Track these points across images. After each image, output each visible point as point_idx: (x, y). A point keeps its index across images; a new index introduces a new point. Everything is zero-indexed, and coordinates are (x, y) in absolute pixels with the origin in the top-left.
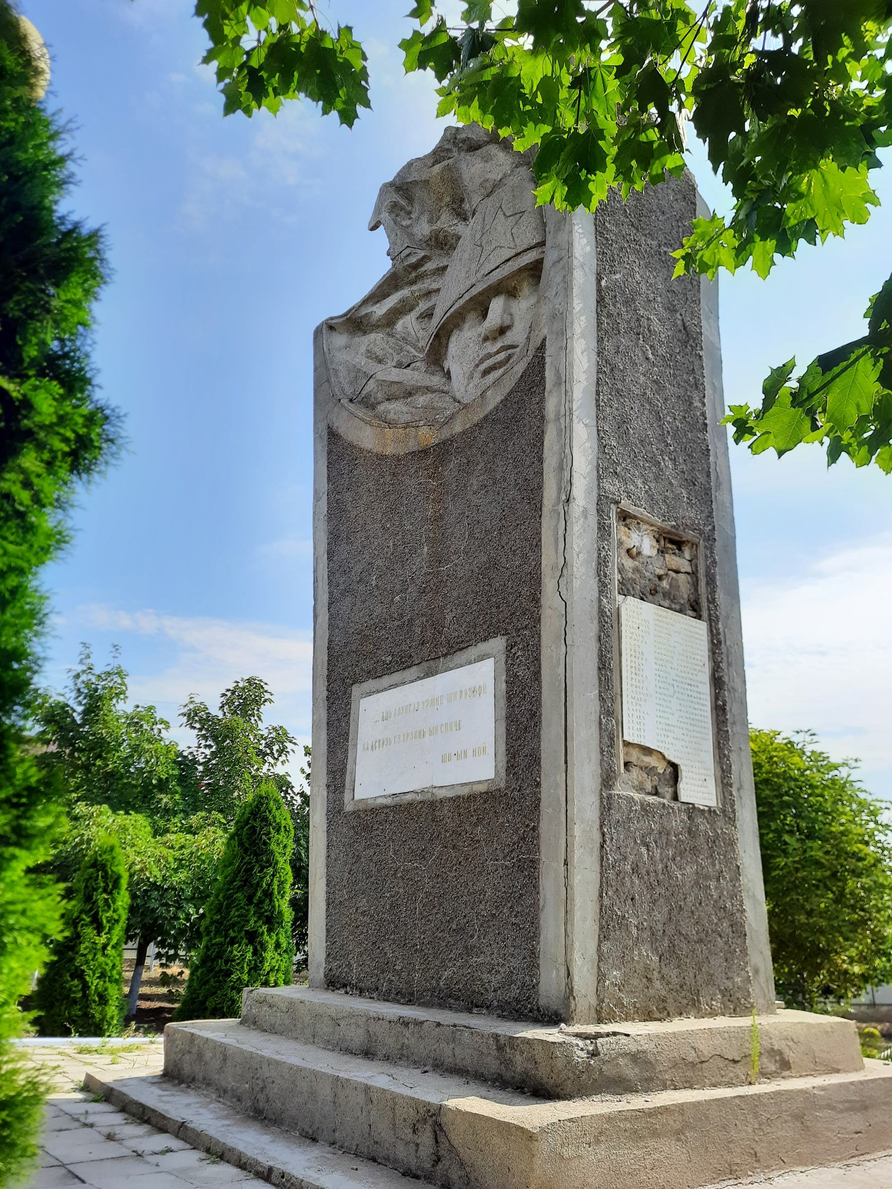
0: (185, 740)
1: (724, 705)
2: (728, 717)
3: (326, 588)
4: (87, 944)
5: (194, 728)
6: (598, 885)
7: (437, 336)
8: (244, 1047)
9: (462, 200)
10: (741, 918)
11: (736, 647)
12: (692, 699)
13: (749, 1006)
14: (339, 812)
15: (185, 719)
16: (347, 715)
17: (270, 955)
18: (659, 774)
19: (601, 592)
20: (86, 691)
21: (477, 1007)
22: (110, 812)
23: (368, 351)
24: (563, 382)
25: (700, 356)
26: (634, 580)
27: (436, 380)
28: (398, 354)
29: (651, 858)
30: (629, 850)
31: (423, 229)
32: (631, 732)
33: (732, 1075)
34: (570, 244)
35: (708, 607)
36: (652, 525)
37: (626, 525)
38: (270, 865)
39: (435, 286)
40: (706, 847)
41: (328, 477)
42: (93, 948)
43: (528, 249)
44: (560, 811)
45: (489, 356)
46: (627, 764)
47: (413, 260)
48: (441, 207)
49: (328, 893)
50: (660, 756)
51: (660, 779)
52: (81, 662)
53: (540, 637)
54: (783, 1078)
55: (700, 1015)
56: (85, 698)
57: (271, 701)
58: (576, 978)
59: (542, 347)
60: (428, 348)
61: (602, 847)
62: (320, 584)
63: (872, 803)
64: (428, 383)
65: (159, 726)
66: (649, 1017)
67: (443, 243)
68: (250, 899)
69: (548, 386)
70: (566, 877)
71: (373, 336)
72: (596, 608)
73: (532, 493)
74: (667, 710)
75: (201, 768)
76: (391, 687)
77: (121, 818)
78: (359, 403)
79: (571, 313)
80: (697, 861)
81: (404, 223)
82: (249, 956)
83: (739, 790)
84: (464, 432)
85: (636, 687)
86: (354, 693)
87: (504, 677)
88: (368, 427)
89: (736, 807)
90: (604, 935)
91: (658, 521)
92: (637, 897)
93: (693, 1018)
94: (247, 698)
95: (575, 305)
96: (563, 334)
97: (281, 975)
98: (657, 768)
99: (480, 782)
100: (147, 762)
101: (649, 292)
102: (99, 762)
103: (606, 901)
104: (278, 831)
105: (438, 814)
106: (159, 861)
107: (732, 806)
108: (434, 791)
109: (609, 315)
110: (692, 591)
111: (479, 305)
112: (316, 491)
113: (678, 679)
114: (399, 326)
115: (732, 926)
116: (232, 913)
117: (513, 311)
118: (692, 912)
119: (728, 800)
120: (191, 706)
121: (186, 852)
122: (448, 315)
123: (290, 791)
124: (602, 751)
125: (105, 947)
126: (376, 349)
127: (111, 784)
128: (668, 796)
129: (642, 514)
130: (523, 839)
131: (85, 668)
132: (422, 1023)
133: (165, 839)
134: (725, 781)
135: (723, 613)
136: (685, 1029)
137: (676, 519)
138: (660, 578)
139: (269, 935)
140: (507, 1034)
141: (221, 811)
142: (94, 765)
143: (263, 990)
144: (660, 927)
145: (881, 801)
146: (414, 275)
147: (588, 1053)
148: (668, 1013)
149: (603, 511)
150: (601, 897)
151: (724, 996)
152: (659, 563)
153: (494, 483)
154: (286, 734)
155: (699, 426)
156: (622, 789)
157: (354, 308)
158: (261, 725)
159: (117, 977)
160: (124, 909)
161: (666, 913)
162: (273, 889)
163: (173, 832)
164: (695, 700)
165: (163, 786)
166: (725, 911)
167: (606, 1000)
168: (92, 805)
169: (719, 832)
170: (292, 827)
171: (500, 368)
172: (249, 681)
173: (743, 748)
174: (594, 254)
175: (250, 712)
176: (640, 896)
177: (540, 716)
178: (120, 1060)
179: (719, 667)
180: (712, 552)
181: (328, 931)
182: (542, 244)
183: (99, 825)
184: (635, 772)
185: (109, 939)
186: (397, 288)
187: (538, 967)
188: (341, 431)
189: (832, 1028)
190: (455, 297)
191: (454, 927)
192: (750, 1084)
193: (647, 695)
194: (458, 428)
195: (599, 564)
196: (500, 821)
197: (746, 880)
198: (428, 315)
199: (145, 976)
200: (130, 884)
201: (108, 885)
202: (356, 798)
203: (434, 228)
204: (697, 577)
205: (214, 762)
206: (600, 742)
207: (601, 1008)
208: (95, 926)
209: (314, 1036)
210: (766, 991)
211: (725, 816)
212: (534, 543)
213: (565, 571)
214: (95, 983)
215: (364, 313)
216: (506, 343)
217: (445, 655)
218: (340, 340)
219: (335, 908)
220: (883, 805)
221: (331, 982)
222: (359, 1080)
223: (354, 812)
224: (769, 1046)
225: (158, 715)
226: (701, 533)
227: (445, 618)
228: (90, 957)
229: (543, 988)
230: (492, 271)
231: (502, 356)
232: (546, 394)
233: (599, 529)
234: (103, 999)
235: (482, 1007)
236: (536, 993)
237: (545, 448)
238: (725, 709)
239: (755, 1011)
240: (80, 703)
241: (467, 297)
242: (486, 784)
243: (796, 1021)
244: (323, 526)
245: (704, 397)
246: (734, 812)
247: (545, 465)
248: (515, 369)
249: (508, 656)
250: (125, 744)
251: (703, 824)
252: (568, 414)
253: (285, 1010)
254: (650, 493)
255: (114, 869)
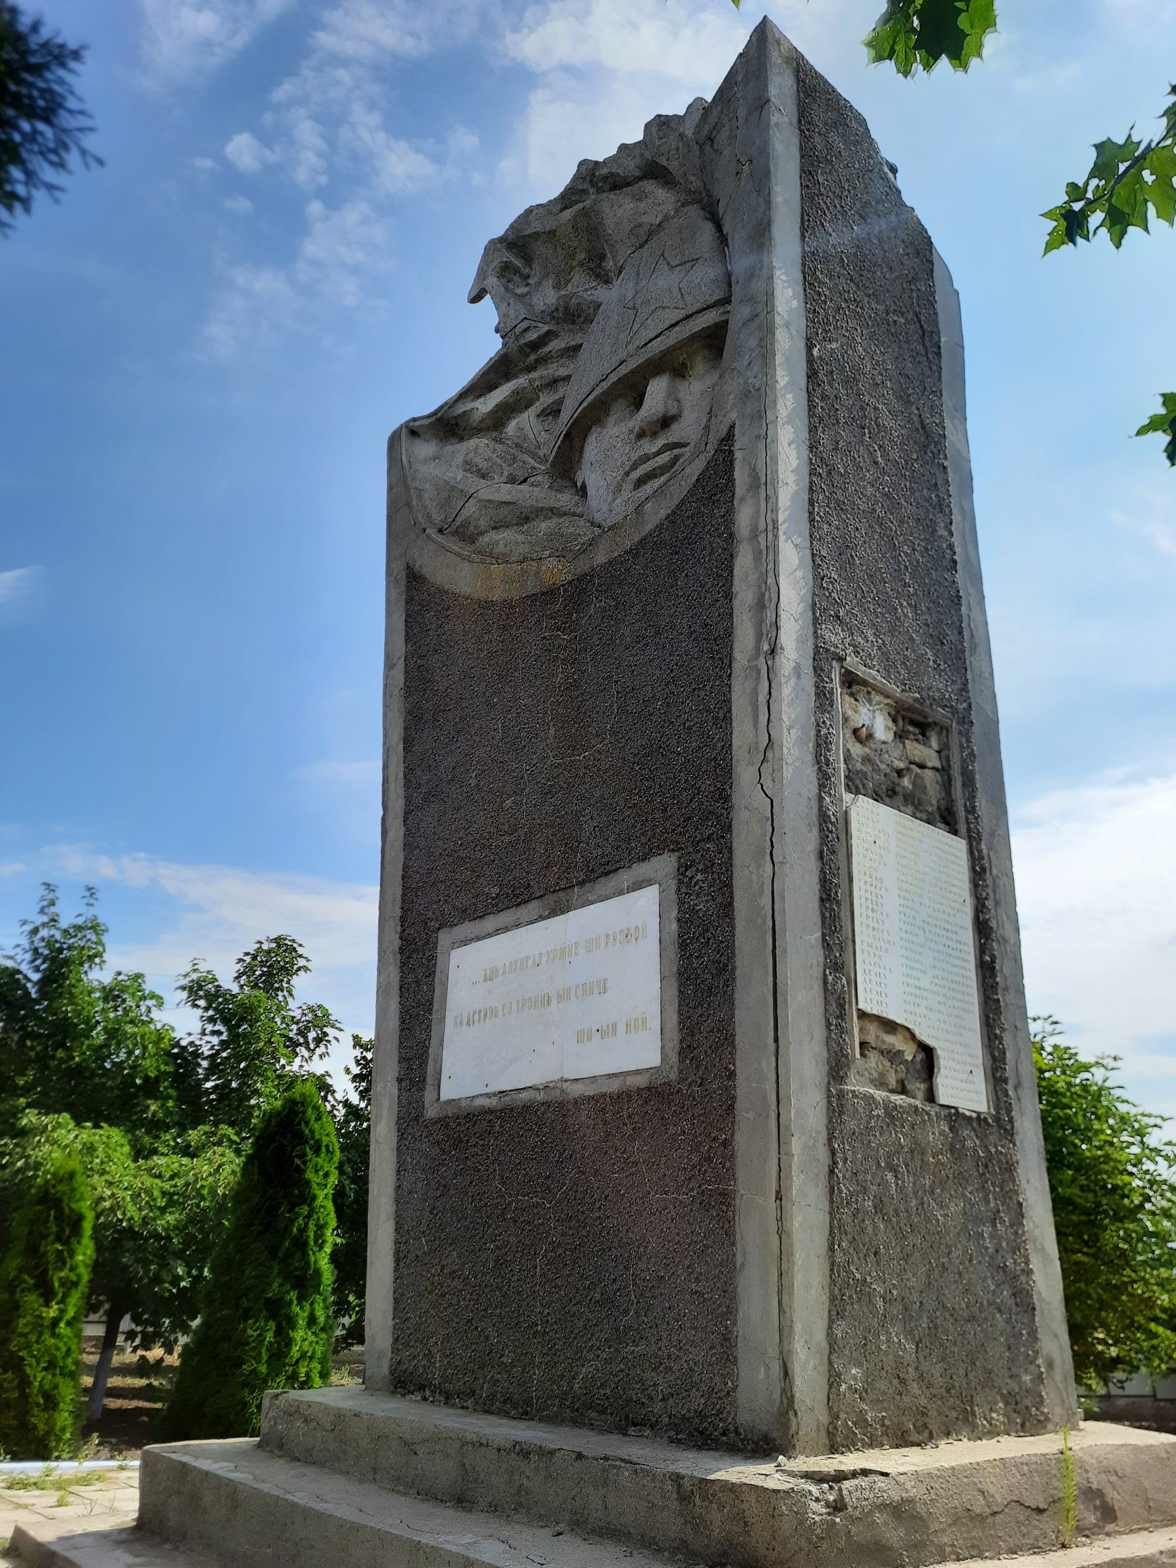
0: (185, 1023)
1: (993, 961)
2: (998, 979)
3: (401, 791)
4: (29, 1318)
5: (197, 1006)
6: (827, 1232)
7: (568, 435)
8: (265, 1487)
9: (603, 257)
10: (1027, 1283)
11: (1005, 878)
12: (950, 951)
13: (1042, 1418)
14: (416, 1119)
15: (185, 994)
16: (431, 974)
17: (302, 1338)
18: (906, 1061)
19: (821, 786)
20: (46, 952)
21: (635, 1425)
22: (72, 1125)
23: (466, 462)
24: (762, 484)
25: (945, 468)
26: (865, 774)
27: (566, 499)
28: (509, 466)
29: (901, 1189)
30: (869, 1177)
31: (547, 297)
32: (869, 996)
33: (1036, 1532)
34: (770, 295)
35: (967, 818)
36: (887, 697)
37: (852, 695)
38: (304, 1202)
39: (563, 372)
40: (976, 1173)
41: (407, 635)
42: (38, 1325)
43: (704, 309)
44: (768, 1116)
45: (646, 458)
46: (863, 1045)
47: (533, 336)
48: (572, 268)
49: (397, 1242)
50: (908, 1035)
51: (907, 1069)
52: (42, 911)
53: (731, 852)
54: (1108, 1534)
55: (977, 1435)
56: (44, 963)
57: (306, 969)
58: (798, 1381)
59: (729, 437)
60: (554, 454)
61: (832, 1172)
62: (392, 786)
63: (1139, 1118)
64: (552, 503)
65: (150, 1003)
66: (902, 1440)
67: (575, 316)
68: (273, 1252)
69: (739, 491)
70: (780, 1220)
71: (474, 442)
72: (815, 810)
73: (717, 644)
74: (916, 965)
75: (205, 1064)
76: (498, 931)
77: (88, 1133)
78: (453, 534)
79: (773, 388)
80: (964, 1196)
81: (518, 291)
82: (270, 1336)
83: (1016, 1088)
84: (610, 563)
85: (874, 929)
86: (440, 943)
87: (674, 913)
88: (467, 564)
89: (1013, 1113)
90: (837, 1310)
91: (897, 691)
92: (882, 1251)
93: (965, 1440)
94: (274, 965)
95: (779, 378)
96: (760, 418)
97: (316, 1365)
98: (903, 1052)
99: (637, 1072)
100: (130, 1053)
101: (875, 373)
102: (60, 1054)
103: (839, 1257)
104: (317, 1151)
105: (570, 1121)
106: (139, 1195)
107: (1009, 1111)
108: (565, 1085)
109: (824, 397)
110: (943, 795)
111: (631, 390)
112: (388, 657)
113: (931, 921)
114: (511, 428)
115: (1014, 1295)
116: (247, 1273)
117: (681, 395)
118: (960, 1273)
119: (1002, 1104)
120: (195, 976)
121: (180, 1182)
122: (585, 404)
123: (330, 1098)
124: (828, 1024)
125: (55, 1322)
126: (477, 460)
127: (77, 1084)
128: (920, 1095)
129: (875, 679)
130: (709, 1160)
131: (45, 919)
132: (552, 1453)
133: (150, 1163)
134: (998, 1075)
135: (985, 827)
136: (966, 1461)
137: (920, 690)
138: (900, 773)
139: (300, 1304)
140: (695, 1474)
141: (231, 1124)
142: (53, 1057)
143: (296, 1395)
144: (915, 1297)
145: (1149, 1116)
146: (533, 357)
147: (828, 1505)
148: (931, 1433)
149: (822, 670)
150: (831, 1249)
151: (1007, 1404)
152: (896, 753)
153: (657, 633)
154: (326, 1015)
155: (946, 563)
156: (856, 1084)
157: (446, 403)
158: (292, 1004)
159: (73, 1368)
160: (86, 1266)
161: (923, 1277)
162: (308, 1237)
163: (162, 1154)
164: (955, 953)
165: (151, 1088)
166: (1005, 1272)
167: (843, 1415)
168: (47, 1114)
169: (993, 1150)
170: (337, 1146)
171: (662, 475)
172: (278, 941)
173: (1019, 1026)
174: (802, 311)
175: (276, 985)
176: (887, 1248)
177: (734, 969)
178: (71, 1499)
179: (984, 906)
180: (968, 741)
181: (396, 1301)
182: (726, 301)
183: (55, 1142)
184: (873, 1057)
185: (62, 1311)
186: (508, 377)
187: (735, 1362)
188: (425, 571)
189: (1168, 1452)
190: (594, 380)
191: (597, 1296)
192: (1064, 1546)
193: (889, 942)
194: (601, 558)
195: (818, 745)
196: (672, 1130)
197: (1031, 1225)
198: (553, 411)
199: (117, 1360)
200: (96, 1228)
201: (64, 1231)
202: (443, 1098)
203: (563, 293)
204: (949, 776)
205: (224, 1054)
206: (826, 1010)
207: (835, 1428)
208: (41, 1291)
209: (375, 1470)
210: (1065, 1395)
211: (1000, 1127)
212: (721, 715)
213: (770, 754)
214: (39, 1376)
215: (460, 411)
216: (671, 440)
217: (582, 883)
218: (425, 449)
219: (408, 1267)
220: (1152, 1121)
221: (399, 1381)
222: (454, 1549)
223: (440, 1120)
224: (1085, 1482)
225: (148, 987)
226: (954, 711)
227: (581, 829)
228: (33, 1338)
229: (743, 1396)
230: (650, 341)
231: (665, 458)
232: (735, 503)
233: (817, 695)
234: (51, 1402)
235: (644, 1425)
236: (733, 1403)
237: (736, 578)
238: (994, 968)
239: (1050, 1426)
240: (37, 969)
241: (613, 378)
242: (647, 1075)
243: (1117, 1443)
244: (397, 704)
245: (951, 523)
246: (1011, 1120)
247: (736, 603)
248: (688, 470)
249: (680, 882)
250: (99, 1028)
251: (971, 1139)
252: (770, 528)
253: (329, 1426)
254: (884, 650)
255: (74, 1206)
